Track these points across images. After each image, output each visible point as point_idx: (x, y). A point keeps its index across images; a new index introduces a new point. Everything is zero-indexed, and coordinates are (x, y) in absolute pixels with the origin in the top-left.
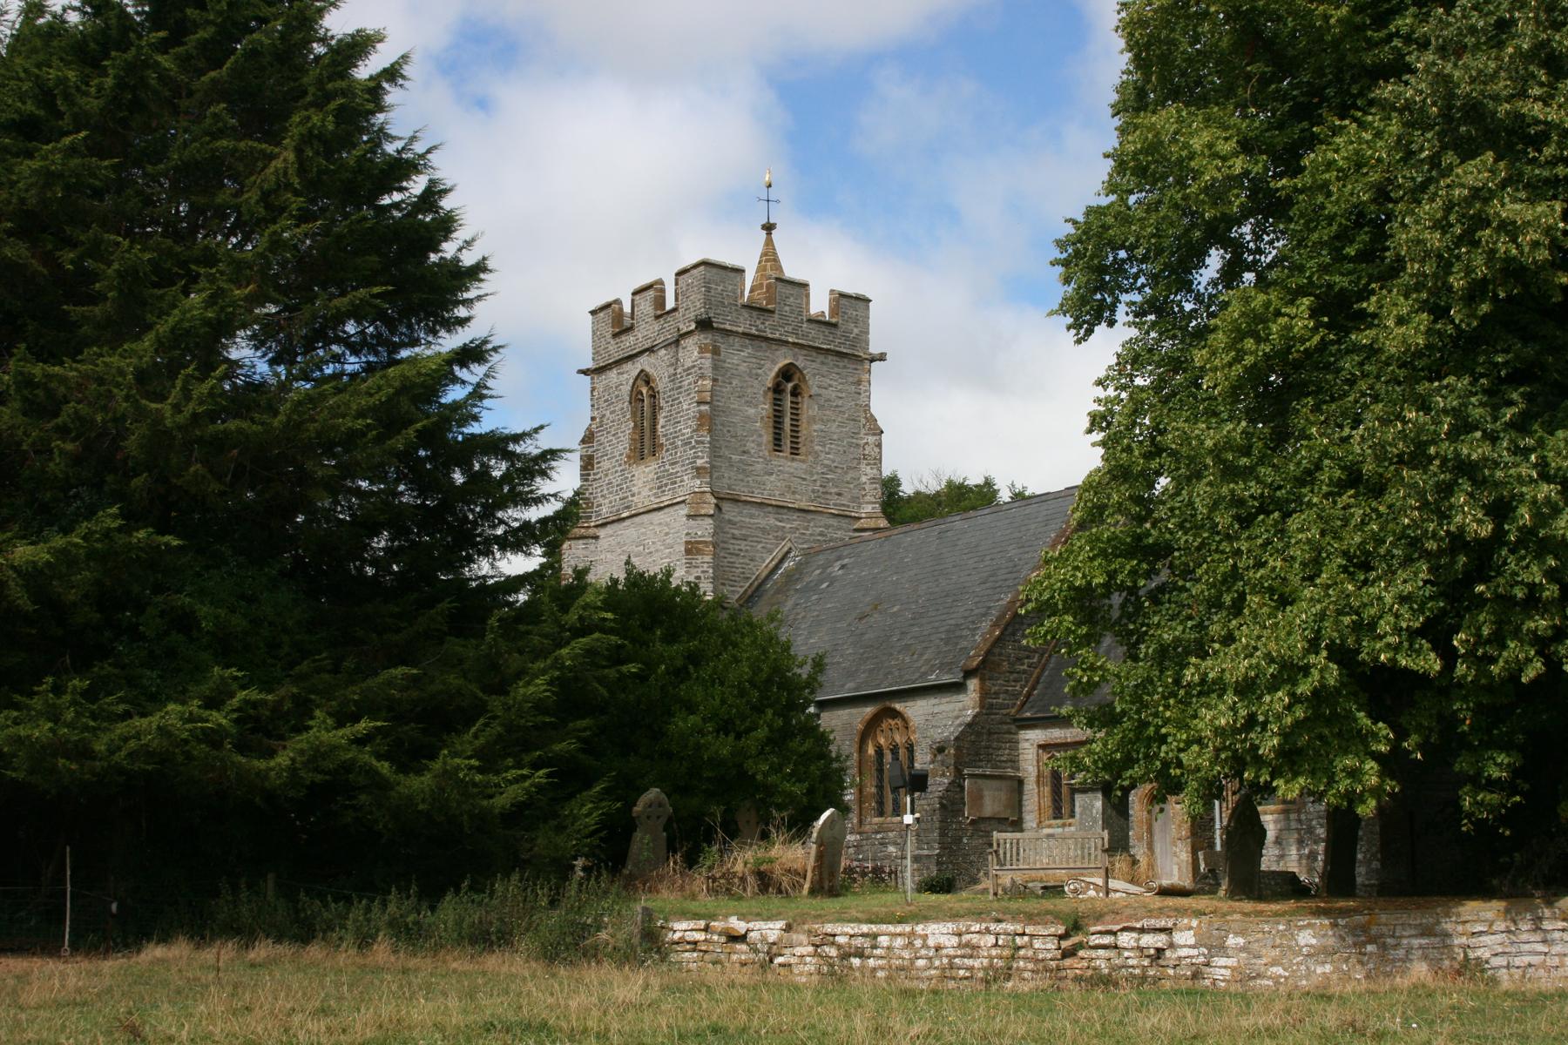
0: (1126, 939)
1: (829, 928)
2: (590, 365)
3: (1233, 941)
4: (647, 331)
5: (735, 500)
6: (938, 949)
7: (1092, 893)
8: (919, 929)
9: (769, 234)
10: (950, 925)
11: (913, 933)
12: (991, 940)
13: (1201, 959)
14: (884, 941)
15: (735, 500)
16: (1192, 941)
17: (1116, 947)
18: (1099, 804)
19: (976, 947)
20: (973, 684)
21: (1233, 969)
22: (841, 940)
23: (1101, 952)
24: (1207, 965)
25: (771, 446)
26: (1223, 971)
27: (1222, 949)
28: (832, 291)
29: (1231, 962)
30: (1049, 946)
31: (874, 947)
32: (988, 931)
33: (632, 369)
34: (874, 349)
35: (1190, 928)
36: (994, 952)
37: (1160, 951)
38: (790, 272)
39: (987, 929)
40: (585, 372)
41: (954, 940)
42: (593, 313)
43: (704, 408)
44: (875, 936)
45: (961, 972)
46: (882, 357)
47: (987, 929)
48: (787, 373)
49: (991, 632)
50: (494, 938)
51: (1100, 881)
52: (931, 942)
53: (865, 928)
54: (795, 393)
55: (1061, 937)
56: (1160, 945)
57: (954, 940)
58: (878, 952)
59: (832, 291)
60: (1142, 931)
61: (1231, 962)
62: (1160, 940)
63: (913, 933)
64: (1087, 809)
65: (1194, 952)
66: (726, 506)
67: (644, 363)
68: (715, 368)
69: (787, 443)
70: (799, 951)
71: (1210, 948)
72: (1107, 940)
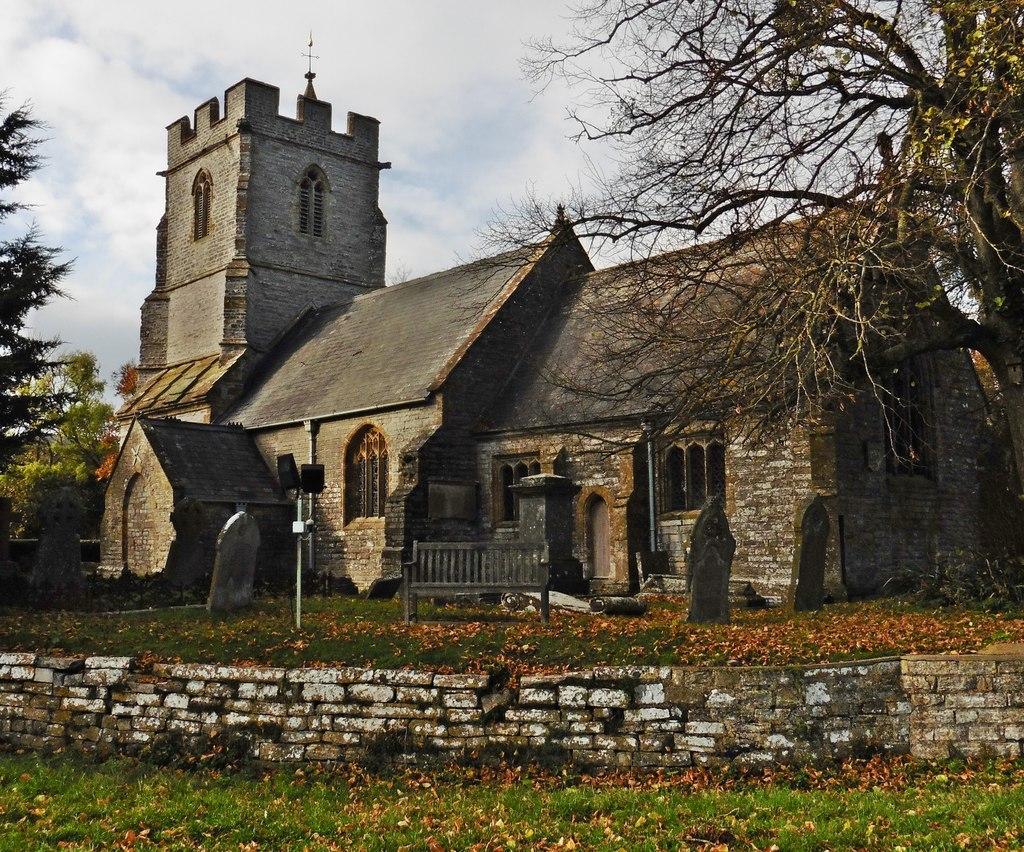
0: (568, 695)
1: (179, 670)
2: (165, 168)
3: (717, 698)
4: (205, 136)
5: (268, 267)
6: (317, 702)
7: (531, 608)
8: (294, 676)
9: (310, 81)
10: (333, 672)
11: (285, 680)
12: (388, 692)
13: (674, 724)
14: (247, 689)
15: (268, 267)
16: (660, 698)
17: (556, 706)
18: (542, 508)
19: (369, 703)
20: (439, 399)
21: (717, 738)
22: (194, 687)
23: (535, 714)
24: (682, 731)
25: (298, 228)
26: (704, 741)
27: (703, 712)
28: (350, 114)
29: (715, 728)
30: (465, 704)
31: (236, 697)
32: (384, 681)
33: (193, 169)
34: (381, 159)
35: (658, 680)
36: (391, 711)
37: (617, 713)
38: (320, 96)
39: (383, 677)
40: (162, 174)
41: (339, 692)
42: (168, 128)
43: (244, 193)
44: (234, 684)
45: (347, 737)
46: (387, 165)
47: (383, 677)
48: (313, 173)
49: (454, 359)
50: (896, 471)
51: (538, 596)
52: (307, 694)
53: (224, 672)
54: (319, 189)
55: (482, 693)
56: (616, 703)
57: (339, 692)
58: (239, 704)
59: (350, 114)
60: (594, 684)
61: (715, 728)
62: (618, 698)
63: (285, 680)
64: (531, 513)
65: (665, 714)
66: (261, 272)
67: (202, 163)
68: (252, 163)
69: (311, 227)
70: (142, 699)
71: (685, 708)
72: (544, 696)
